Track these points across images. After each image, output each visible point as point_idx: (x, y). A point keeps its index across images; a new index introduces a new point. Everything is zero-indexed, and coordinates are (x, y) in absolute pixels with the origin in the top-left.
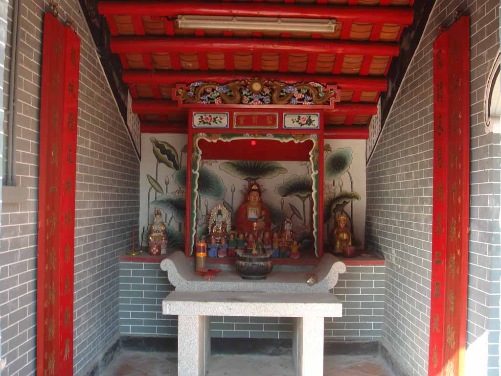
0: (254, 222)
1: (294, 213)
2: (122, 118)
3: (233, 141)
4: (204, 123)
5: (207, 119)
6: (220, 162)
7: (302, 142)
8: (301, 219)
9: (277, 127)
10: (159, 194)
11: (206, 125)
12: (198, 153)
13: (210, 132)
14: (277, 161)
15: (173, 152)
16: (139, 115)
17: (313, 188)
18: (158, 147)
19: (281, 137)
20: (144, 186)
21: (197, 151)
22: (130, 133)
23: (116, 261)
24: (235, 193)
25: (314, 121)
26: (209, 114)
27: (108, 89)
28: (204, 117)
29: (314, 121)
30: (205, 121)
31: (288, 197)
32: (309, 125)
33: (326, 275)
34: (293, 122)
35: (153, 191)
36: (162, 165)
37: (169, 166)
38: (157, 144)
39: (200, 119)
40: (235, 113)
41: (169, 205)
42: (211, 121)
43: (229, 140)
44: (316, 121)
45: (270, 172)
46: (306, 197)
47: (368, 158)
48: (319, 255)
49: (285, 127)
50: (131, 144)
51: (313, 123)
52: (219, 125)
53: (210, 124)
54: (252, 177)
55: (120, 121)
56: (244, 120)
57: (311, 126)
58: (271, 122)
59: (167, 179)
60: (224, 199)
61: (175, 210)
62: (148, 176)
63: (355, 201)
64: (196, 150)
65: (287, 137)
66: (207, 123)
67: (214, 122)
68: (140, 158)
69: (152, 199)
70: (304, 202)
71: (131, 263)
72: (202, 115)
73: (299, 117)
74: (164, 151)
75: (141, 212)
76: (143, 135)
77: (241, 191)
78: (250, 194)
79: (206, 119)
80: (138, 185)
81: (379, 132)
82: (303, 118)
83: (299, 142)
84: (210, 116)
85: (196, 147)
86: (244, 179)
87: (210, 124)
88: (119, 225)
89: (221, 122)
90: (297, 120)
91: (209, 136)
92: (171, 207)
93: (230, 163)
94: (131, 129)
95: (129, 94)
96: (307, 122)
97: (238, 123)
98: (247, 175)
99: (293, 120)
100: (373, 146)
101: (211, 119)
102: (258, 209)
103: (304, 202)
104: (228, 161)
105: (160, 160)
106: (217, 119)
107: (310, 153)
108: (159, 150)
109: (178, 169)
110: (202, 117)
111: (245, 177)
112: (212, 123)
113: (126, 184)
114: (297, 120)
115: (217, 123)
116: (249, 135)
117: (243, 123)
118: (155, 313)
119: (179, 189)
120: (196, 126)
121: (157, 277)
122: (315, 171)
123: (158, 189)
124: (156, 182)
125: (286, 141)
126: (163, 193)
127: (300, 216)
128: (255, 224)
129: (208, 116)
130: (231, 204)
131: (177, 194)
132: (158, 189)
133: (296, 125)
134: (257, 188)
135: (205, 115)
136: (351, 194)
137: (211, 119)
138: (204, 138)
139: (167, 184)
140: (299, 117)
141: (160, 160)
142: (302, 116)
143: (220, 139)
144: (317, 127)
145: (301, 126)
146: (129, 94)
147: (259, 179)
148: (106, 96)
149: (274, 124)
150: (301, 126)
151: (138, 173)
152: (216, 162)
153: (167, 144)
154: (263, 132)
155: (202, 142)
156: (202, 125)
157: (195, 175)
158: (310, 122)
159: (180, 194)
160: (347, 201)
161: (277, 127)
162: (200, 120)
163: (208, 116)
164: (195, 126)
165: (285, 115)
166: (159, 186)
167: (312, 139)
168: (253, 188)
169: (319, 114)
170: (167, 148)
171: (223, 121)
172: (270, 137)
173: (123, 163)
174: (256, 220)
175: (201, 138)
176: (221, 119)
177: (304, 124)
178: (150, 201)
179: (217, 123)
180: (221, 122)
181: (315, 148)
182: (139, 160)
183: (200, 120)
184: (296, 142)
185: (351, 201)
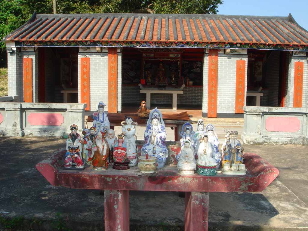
171: (152, 55)
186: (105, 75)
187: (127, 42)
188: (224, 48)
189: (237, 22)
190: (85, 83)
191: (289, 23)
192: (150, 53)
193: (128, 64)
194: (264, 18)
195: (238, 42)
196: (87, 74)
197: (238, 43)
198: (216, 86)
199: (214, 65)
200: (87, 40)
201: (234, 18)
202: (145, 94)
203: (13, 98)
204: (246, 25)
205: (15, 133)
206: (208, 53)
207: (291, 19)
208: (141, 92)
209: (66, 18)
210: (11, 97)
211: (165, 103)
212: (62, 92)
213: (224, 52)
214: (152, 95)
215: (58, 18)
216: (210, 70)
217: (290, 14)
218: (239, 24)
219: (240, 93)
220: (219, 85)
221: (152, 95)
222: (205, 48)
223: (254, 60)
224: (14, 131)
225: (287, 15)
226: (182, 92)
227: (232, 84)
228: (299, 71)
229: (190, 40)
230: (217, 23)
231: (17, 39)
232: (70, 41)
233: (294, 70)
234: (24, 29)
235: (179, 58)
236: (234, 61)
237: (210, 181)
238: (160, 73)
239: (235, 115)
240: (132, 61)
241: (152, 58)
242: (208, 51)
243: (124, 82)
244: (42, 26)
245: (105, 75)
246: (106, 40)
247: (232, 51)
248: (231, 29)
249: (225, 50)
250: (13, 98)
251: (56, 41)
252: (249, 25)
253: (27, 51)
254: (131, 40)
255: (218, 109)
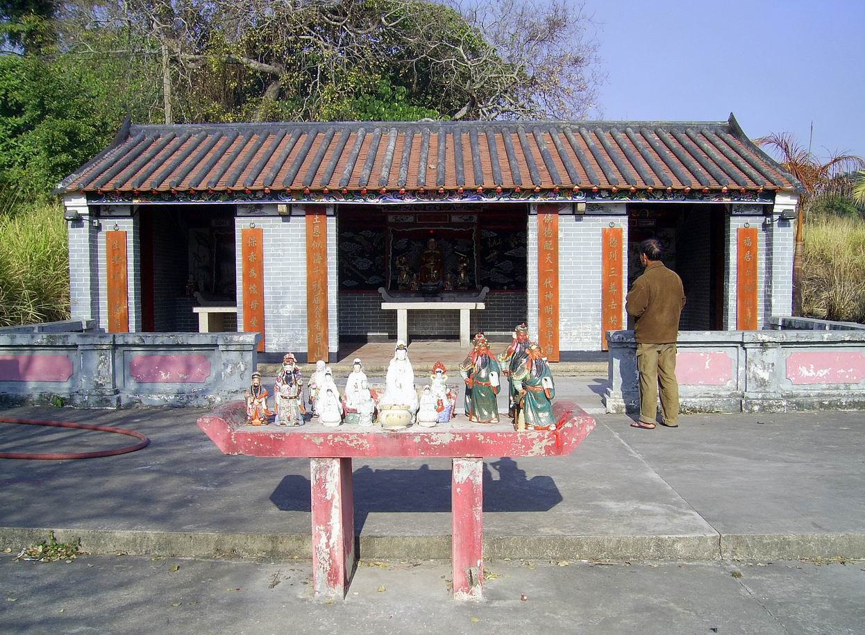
44: (475, 218)
154: (439, 225)
171: (411, 219)
186: (298, 269)
187: (349, 192)
188: (572, 200)
189: (606, 136)
190: (253, 287)
191: (729, 137)
192: (405, 214)
193: (351, 240)
194: (673, 129)
195: (603, 186)
196: (256, 265)
197: (604, 189)
198: (554, 289)
199: (550, 241)
200: (253, 188)
201: (599, 129)
202: (457, 312)
203: (84, 323)
204: (625, 146)
205: (101, 401)
206: (536, 213)
207: (733, 128)
208: (385, 306)
209: (203, 133)
210: (80, 323)
211: (442, 332)
212: (196, 310)
213: (574, 211)
214: (410, 313)
215: (184, 136)
216: (542, 252)
217: (732, 120)
218: (609, 143)
219: (613, 304)
220: (561, 287)
221: (410, 313)
222: (529, 203)
223: (653, 224)
224: (98, 395)
225: (725, 119)
226: (481, 306)
227: (781, 288)
228: (748, 248)
229: (493, 186)
230: (559, 142)
231: (90, 187)
232: (216, 191)
233: (736, 247)
234: (102, 164)
235: (473, 224)
236: (595, 227)
237: (482, 438)
238: (430, 262)
239: (602, 353)
240: (363, 233)
241: (409, 225)
242: (536, 208)
243: (343, 283)
244: (147, 154)
245: (298, 269)
246: (298, 188)
247: (589, 206)
248: (589, 156)
249: (574, 205)
250: (84, 323)
251: (183, 192)
252: (633, 143)
253: (114, 214)
254: (357, 188)
255: (594, 349)
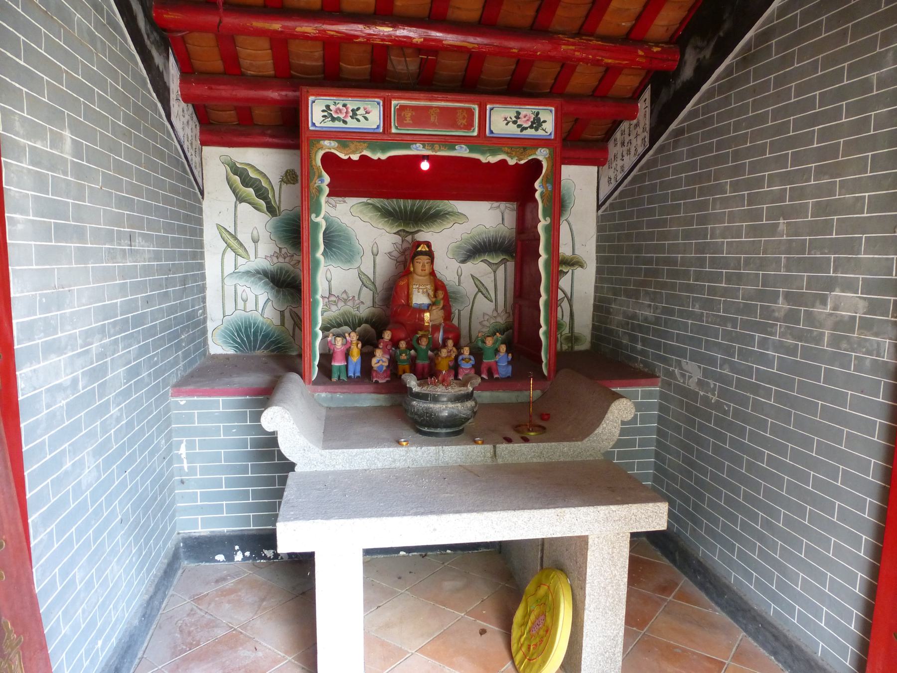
0: (424, 311)
1: (480, 291)
2: (159, 105)
3: (390, 158)
4: (333, 119)
5: (338, 111)
6: (352, 201)
7: (522, 162)
8: (492, 301)
9: (475, 134)
10: (241, 260)
11: (338, 124)
12: (322, 181)
13: (344, 137)
14: (451, 202)
15: (264, 184)
16: (194, 106)
17: (542, 250)
18: (235, 174)
19: (483, 153)
20: (210, 235)
21: (320, 176)
22: (179, 142)
23: (164, 397)
24: (378, 258)
25: (545, 122)
26: (342, 103)
27: (118, 24)
28: (332, 107)
29: (545, 122)
30: (335, 116)
31: (469, 264)
32: (537, 129)
33: (598, 426)
34: (507, 124)
35: (230, 255)
36: (244, 207)
37: (257, 207)
38: (235, 170)
39: (323, 111)
40: (394, 102)
41: (260, 279)
42: (346, 116)
43: (384, 157)
45: (438, 221)
46: (498, 264)
47: (602, 198)
48: (549, 372)
49: (491, 132)
50: (182, 163)
51: (544, 126)
52: (363, 125)
53: (345, 122)
54: (408, 229)
55: (156, 110)
56: (411, 116)
57: (540, 132)
58: (464, 122)
59: (255, 233)
60: (359, 267)
61: (273, 288)
62: (219, 226)
63: (578, 271)
64: (317, 174)
65: (494, 153)
66: (338, 119)
67: (352, 117)
68: (202, 193)
69: (229, 268)
70: (495, 272)
71: (196, 398)
72: (328, 103)
73: (518, 113)
74: (247, 181)
75: (209, 293)
76: (206, 149)
77: (390, 253)
78: (415, 261)
79: (336, 112)
80: (201, 245)
81: (641, 150)
82: (525, 117)
83: (517, 163)
84: (344, 105)
85: (318, 168)
86: (395, 233)
87: (345, 122)
88: (166, 326)
89: (366, 119)
90: (514, 119)
91: (343, 146)
92: (266, 284)
93: (369, 204)
94: (181, 134)
95: (171, 58)
96: (533, 123)
97: (401, 122)
98: (399, 226)
99: (506, 119)
100: (620, 177)
101: (347, 113)
102: (429, 287)
103: (495, 272)
104: (364, 200)
105: (240, 199)
106: (358, 113)
107: (537, 185)
108: (237, 178)
109: (276, 215)
110: (328, 107)
111: (395, 230)
112: (349, 119)
113: (176, 243)
114: (514, 119)
115: (358, 120)
116: (422, 146)
117: (411, 122)
118: (249, 490)
119: (278, 252)
120: (317, 124)
121: (248, 423)
122: (545, 218)
123: (240, 251)
124: (236, 238)
125: (493, 159)
126: (248, 258)
127: (487, 294)
128: (427, 316)
129: (340, 106)
130: (372, 279)
131: (275, 260)
132: (240, 251)
133: (512, 130)
134: (427, 249)
135: (335, 104)
136: (572, 260)
137: (347, 113)
138: (333, 151)
139: (255, 241)
140: (518, 113)
141: (240, 199)
142: (523, 112)
143: (367, 153)
144: (550, 134)
145: (522, 131)
146: (171, 58)
147: (420, 233)
148: (113, 41)
149: (469, 126)
150: (522, 131)
151: (200, 222)
152: (345, 202)
153: (252, 167)
154: (450, 142)
155: (329, 160)
156: (329, 124)
157: (317, 225)
158: (537, 123)
159: (281, 260)
160: (565, 270)
161: (475, 134)
162: (326, 114)
163: (340, 106)
164: (314, 124)
165: (491, 109)
166: (241, 245)
167: (540, 158)
168: (419, 249)
169: (553, 109)
170: (253, 174)
172: (462, 151)
173: (166, 200)
174: (429, 308)
175: (327, 150)
176: (367, 113)
177: (526, 128)
178: (226, 274)
179: (358, 120)
180: (366, 119)
181: (546, 175)
182: (200, 197)
183: (326, 114)
184: (512, 162)
185: (570, 271)
